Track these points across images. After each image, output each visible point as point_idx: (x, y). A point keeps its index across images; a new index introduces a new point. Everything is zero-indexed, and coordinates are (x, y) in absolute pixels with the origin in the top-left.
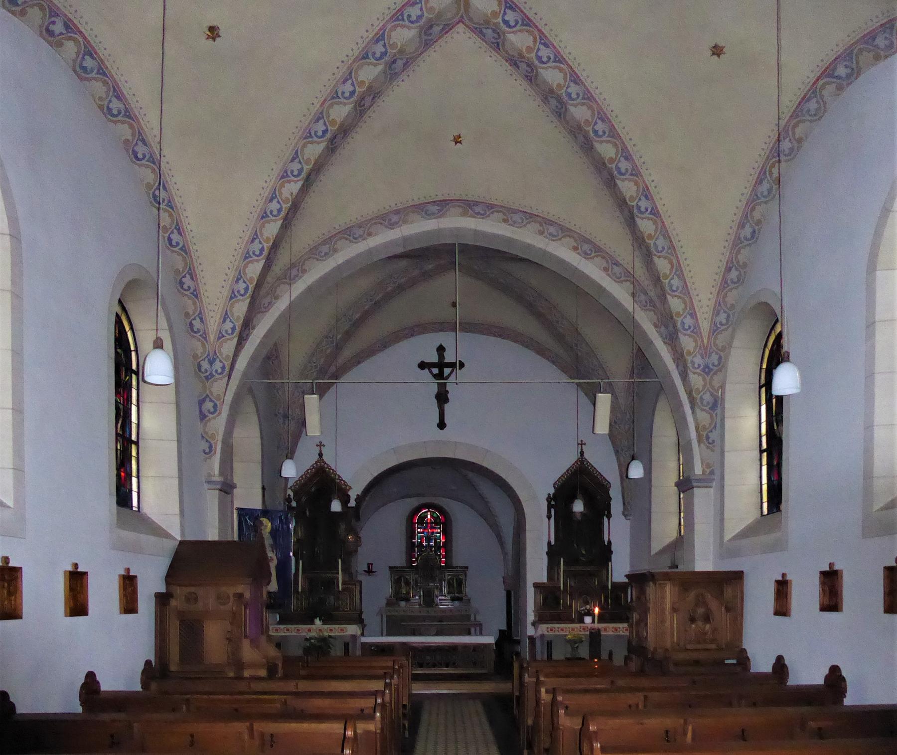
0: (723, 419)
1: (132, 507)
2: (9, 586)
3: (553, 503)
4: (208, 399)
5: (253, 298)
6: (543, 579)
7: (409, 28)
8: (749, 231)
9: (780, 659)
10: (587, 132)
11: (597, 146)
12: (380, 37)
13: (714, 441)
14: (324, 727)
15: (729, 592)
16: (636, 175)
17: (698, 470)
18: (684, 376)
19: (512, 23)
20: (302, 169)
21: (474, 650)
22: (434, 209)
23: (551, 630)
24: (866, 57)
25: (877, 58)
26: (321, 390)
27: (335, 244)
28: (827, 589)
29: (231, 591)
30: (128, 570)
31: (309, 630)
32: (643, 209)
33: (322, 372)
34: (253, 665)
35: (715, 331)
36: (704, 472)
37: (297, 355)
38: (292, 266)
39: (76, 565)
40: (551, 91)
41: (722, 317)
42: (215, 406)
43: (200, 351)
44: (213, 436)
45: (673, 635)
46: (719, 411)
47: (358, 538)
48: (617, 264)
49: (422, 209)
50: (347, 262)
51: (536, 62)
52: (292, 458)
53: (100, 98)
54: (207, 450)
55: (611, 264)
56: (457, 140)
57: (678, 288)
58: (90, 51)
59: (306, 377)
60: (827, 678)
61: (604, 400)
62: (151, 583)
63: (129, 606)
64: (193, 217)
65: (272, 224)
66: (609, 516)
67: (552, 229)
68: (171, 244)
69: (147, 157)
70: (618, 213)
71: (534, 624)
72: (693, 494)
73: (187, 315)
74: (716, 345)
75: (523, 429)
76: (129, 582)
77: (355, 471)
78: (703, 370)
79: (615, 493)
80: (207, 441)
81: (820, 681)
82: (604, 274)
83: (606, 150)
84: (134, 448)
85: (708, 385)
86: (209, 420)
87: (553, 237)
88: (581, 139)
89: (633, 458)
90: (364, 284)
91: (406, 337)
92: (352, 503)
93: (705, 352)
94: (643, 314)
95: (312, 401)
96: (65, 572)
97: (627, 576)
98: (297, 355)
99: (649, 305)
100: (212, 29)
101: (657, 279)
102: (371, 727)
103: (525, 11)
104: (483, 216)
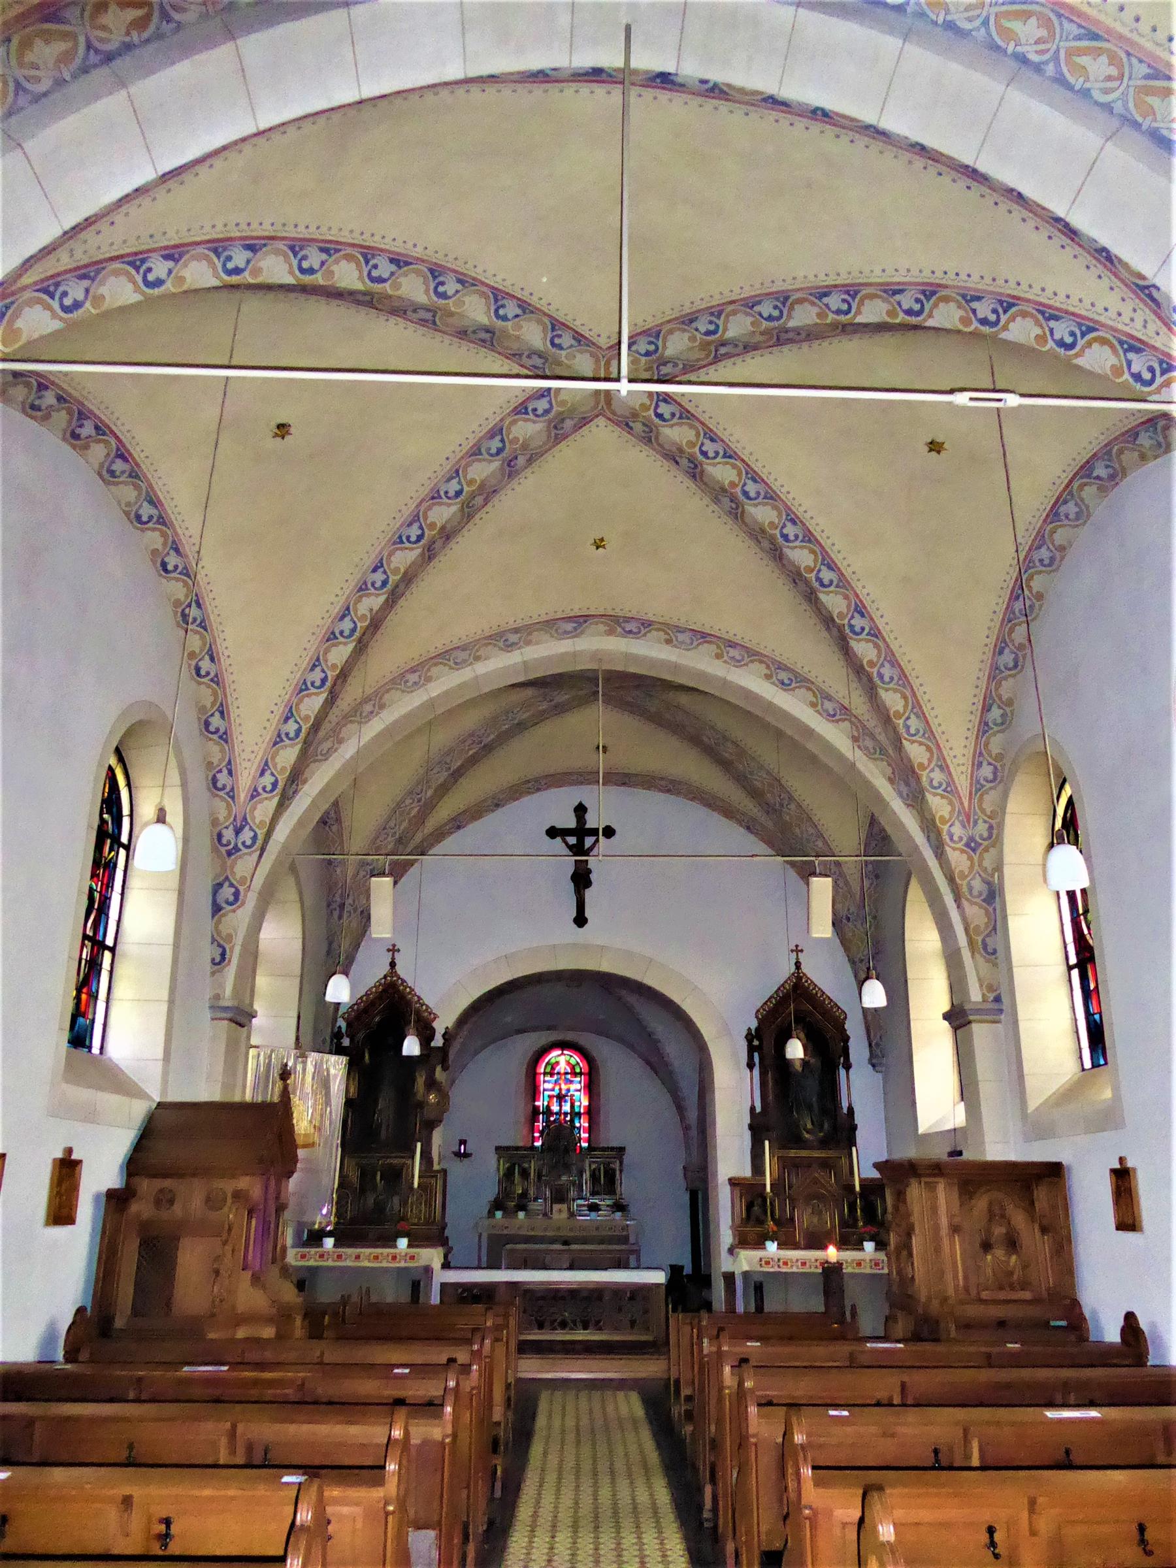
0: (1005, 918)
1: (90, 1048)
3: (756, 1043)
4: (227, 884)
5: (307, 744)
6: (745, 1171)
7: (534, 422)
8: (1014, 646)
9: (1130, 1317)
12: (497, 431)
15: (1041, 1195)
17: (975, 995)
18: (940, 853)
20: (326, 677)
21: (632, 1298)
22: (569, 626)
24: (1129, 457)
25: (1143, 457)
26: (397, 872)
27: (429, 670)
29: (228, 1186)
30: (69, 1151)
31: (358, 1257)
34: (250, 1318)
37: (364, 821)
38: (366, 700)
40: (724, 490)
41: (986, 771)
42: (236, 894)
43: (222, 814)
44: (229, 938)
45: (956, 1277)
47: (444, 1097)
48: (829, 698)
49: (550, 625)
50: (446, 693)
53: (128, 504)
54: (218, 959)
55: (820, 697)
56: (599, 544)
57: (918, 731)
58: (122, 455)
61: (822, 888)
62: (102, 1173)
63: (61, 1212)
64: (232, 636)
66: (848, 1067)
67: (734, 652)
68: (198, 675)
70: (825, 634)
71: (731, 1251)
72: (970, 1035)
73: (210, 765)
76: (67, 1170)
77: (445, 991)
80: (219, 945)
83: (801, 557)
84: (107, 955)
85: (976, 867)
86: (224, 915)
87: (738, 663)
89: (868, 978)
90: (471, 721)
91: (529, 792)
92: (438, 1042)
93: (968, 819)
94: (871, 765)
95: (382, 886)
97: (877, 1166)
98: (364, 821)
99: (877, 752)
100: (280, 426)
101: (886, 719)
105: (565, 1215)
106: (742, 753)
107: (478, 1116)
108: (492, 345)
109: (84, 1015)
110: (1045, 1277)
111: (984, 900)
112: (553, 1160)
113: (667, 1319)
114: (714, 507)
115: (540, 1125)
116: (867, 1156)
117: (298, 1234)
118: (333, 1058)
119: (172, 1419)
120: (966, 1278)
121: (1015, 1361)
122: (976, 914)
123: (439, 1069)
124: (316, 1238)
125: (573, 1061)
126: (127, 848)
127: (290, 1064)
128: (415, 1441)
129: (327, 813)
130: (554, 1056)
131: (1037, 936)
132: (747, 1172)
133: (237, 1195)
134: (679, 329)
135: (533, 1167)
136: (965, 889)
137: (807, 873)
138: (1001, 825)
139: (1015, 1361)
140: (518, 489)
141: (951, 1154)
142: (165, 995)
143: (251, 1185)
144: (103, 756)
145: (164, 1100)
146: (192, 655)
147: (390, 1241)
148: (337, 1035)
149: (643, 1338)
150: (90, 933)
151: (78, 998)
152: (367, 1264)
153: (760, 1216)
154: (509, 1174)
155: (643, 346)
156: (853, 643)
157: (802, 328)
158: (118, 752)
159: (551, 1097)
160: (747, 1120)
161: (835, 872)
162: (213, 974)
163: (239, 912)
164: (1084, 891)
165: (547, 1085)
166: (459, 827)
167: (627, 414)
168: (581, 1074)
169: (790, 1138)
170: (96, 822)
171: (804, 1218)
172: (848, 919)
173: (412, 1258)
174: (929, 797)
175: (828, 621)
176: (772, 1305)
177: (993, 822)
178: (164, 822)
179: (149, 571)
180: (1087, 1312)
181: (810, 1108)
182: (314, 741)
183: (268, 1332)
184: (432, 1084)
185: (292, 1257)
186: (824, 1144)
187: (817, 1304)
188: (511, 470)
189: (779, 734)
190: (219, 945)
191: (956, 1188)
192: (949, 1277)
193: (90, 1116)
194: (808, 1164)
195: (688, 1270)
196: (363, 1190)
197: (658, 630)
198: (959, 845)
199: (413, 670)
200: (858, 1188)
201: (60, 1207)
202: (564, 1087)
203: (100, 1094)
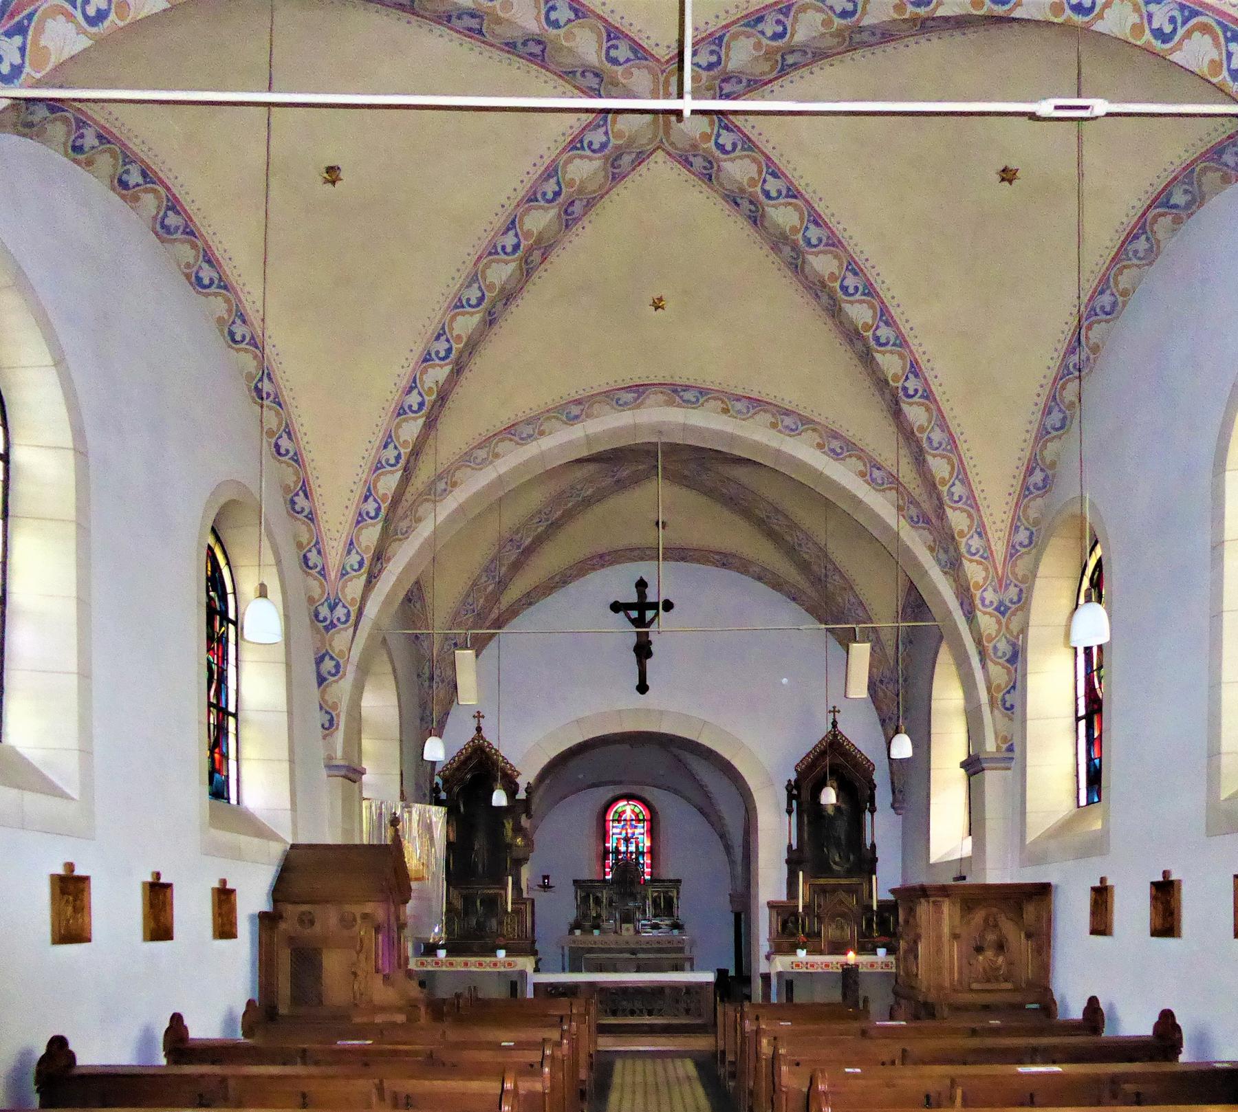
0: (1025, 675)
1: (228, 799)
2: (75, 900)
3: (795, 792)
4: (327, 658)
6: (783, 897)
7: (590, 159)
8: (1059, 414)
9: (1093, 1001)
10: (832, 290)
11: (847, 307)
12: (551, 172)
13: (1012, 706)
14: (475, 1086)
16: (901, 346)
17: (990, 746)
18: (970, 616)
19: (729, 147)
20: (399, 454)
22: (630, 396)
23: (798, 966)
26: (479, 644)
28: (1160, 907)
29: (357, 910)
30: (224, 882)
32: (911, 392)
33: (480, 619)
34: (382, 1009)
35: (1012, 556)
36: (998, 748)
37: (446, 596)
38: (440, 477)
39: (158, 875)
41: (1022, 536)
42: (337, 666)
43: (316, 593)
44: (335, 706)
46: (1019, 665)
47: (529, 844)
51: (762, 197)
52: (440, 735)
53: (188, 265)
54: (327, 725)
55: (871, 469)
58: (174, 205)
59: (459, 625)
60: (1157, 1027)
61: (861, 652)
62: (253, 898)
63: (225, 928)
65: (412, 422)
66: (873, 811)
69: (247, 339)
71: (768, 957)
74: (1014, 573)
75: (755, 696)
76: (224, 897)
77: (526, 750)
78: (997, 609)
79: (881, 777)
80: (327, 712)
81: (1149, 1031)
82: (860, 481)
84: (231, 720)
85: (1004, 629)
87: (792, 431)
88: (825, 299)
89: (897, 732)
90: (536, 499)
92: (521, 795)
93: (1001, 584)
94: (913, 533)
95: (465, 658)
96: (144, 884)
97: (893, 891)
98: (446, 596)
99: (921, 521)
100: (331, 170)
101: (931, 485)
102: (538, 1087)
103: (745, 131)
104: (693, 404)
105: (632, 932)
106: (793, 526)
107: (558, 853)
108: (543, 60)
109: (219, 772)
110: (1027, 971)
111: (1008, 661)
112: (621, 889)
113: (715, 1009)
114: (773, 256)
115: (610, 862)
116: (885, 882)
117: (416, 949)
118: (434, 808)
119: (332, 1077)
120: (960, 973)
121: (995, 1032)
122: (998, 673)
123: (524, 817)
124: (431, 949)
125: (637, 810)
126: (235, 623)
127: (398, 813)
128: (522, 1092)
129: (410, 591)
130: (621, 805)
131: (1052, 688)
132: (783, 897)
133: (365, 916)
134: (743, 33)
135: (604, 895)
136: (991, 651)
137: (846, 639)
138: (1030, 589)
139: (995, 1032)
140: (576, 240)
141: (956, 879)
142: (285, 754)
143: (376, 909)
144: (201, 536)
145: (296, 842)
146: (271, 433)
147: (492, 952)
148: (436, 790)
149: (699, 1021)
150: (213, 700)
151: (212, 757)
152: (473, 969)
153: (792, 929)
154: (585, 899)
155: (704, 59)
156: (905, 407)
157: (874, 26)
158: (214, 531)
159: (618, 839)
160: (785, 855)
161: (873, 636)
162: (324, 737)
163: (341, 682)
164: (1100, 647)
165: (615, 830)
166: (531, 604)
167: (688, 147)
168: (644, 820)
169: (820, 868)
170: (204, 599)
171: (829, 932)
172: (881, 682)
173: (510, 964)
174: (966, 563)
175: (881, 383)
176: (800, 997)
177: (1023, 586)
178: (266, 597)
179: (218, 342)
180: (1057, 997)
181: (838, 845)
182: (394, 516)
183: (400, 1018)
184: (518, 829)
185: (413, 965)
186: (849, 873)
187: (836, 996)
188: (568, 220)
189: (828, 504)
190: (327, 712)
191: (958, 906)
192: (946, 974)
193: (236, 854)
194: (835, 889)
195: (732, 973)
196: (466, 913)
197: (715, 399)
198: (990, 610)
199: (480, 446)
200: (875, 908)
201: (223, 925)
202: (630, 831)
203: (242, 837)
